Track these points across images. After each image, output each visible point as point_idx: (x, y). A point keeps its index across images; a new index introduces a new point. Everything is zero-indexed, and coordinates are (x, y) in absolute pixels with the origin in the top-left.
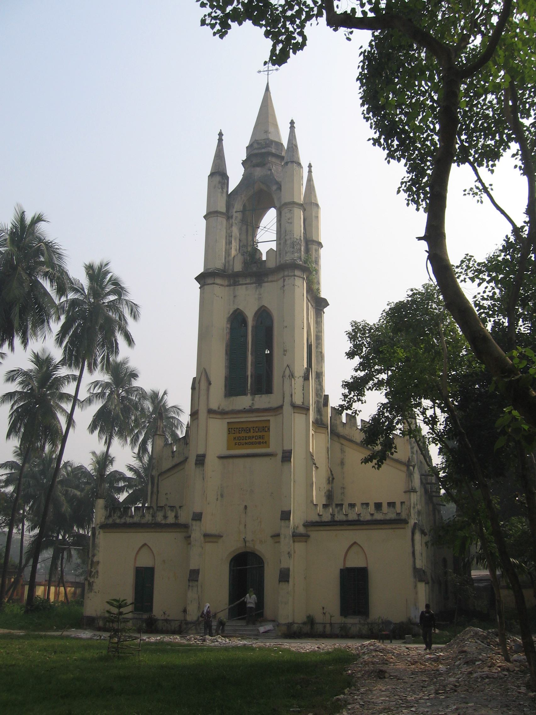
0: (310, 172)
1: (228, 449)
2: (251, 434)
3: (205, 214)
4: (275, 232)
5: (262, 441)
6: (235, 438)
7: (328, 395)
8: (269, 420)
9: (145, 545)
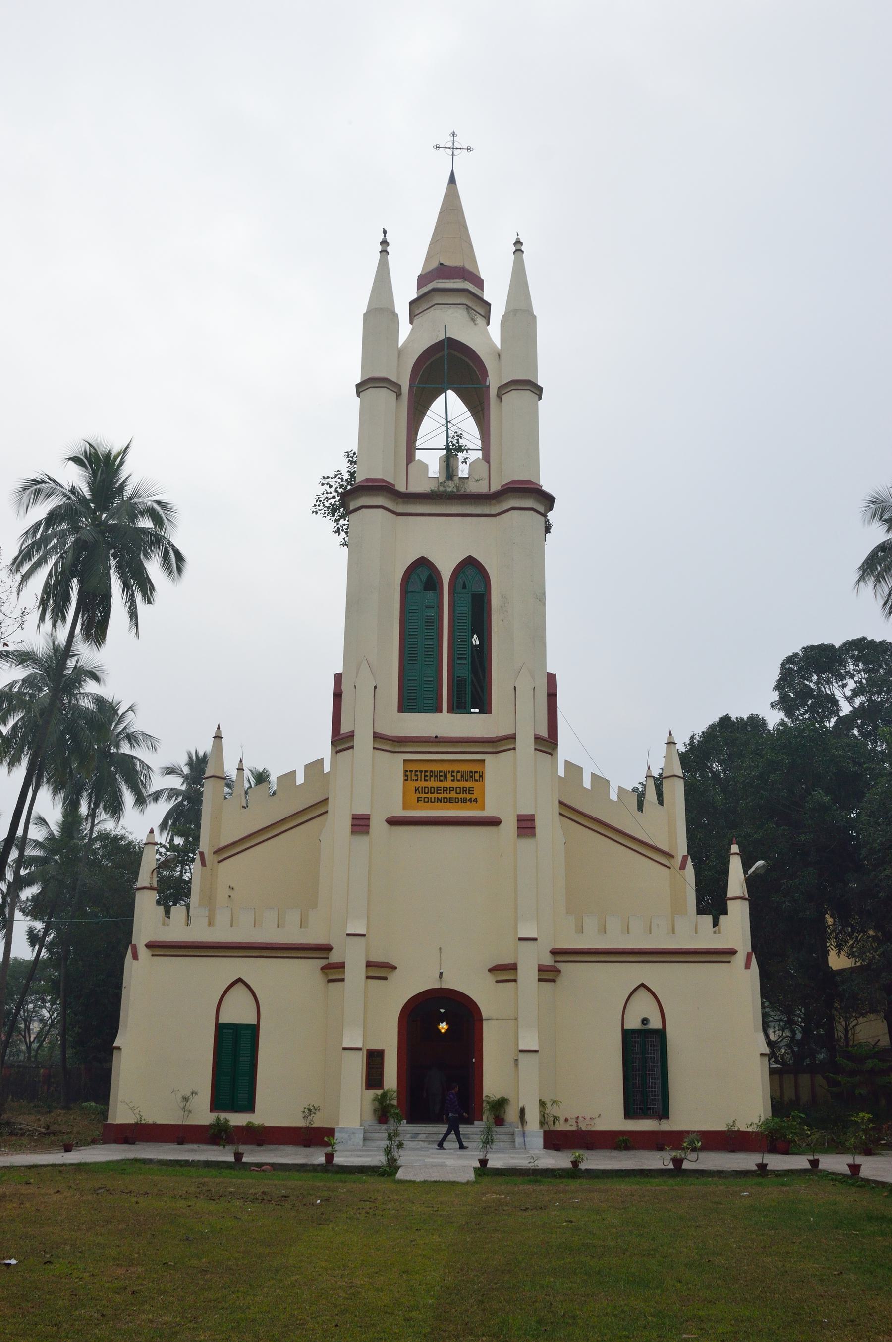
1: (405, 807)
2: (448, 784)
5: (468, 796)
6: (417, 789)
8: (483, 761)
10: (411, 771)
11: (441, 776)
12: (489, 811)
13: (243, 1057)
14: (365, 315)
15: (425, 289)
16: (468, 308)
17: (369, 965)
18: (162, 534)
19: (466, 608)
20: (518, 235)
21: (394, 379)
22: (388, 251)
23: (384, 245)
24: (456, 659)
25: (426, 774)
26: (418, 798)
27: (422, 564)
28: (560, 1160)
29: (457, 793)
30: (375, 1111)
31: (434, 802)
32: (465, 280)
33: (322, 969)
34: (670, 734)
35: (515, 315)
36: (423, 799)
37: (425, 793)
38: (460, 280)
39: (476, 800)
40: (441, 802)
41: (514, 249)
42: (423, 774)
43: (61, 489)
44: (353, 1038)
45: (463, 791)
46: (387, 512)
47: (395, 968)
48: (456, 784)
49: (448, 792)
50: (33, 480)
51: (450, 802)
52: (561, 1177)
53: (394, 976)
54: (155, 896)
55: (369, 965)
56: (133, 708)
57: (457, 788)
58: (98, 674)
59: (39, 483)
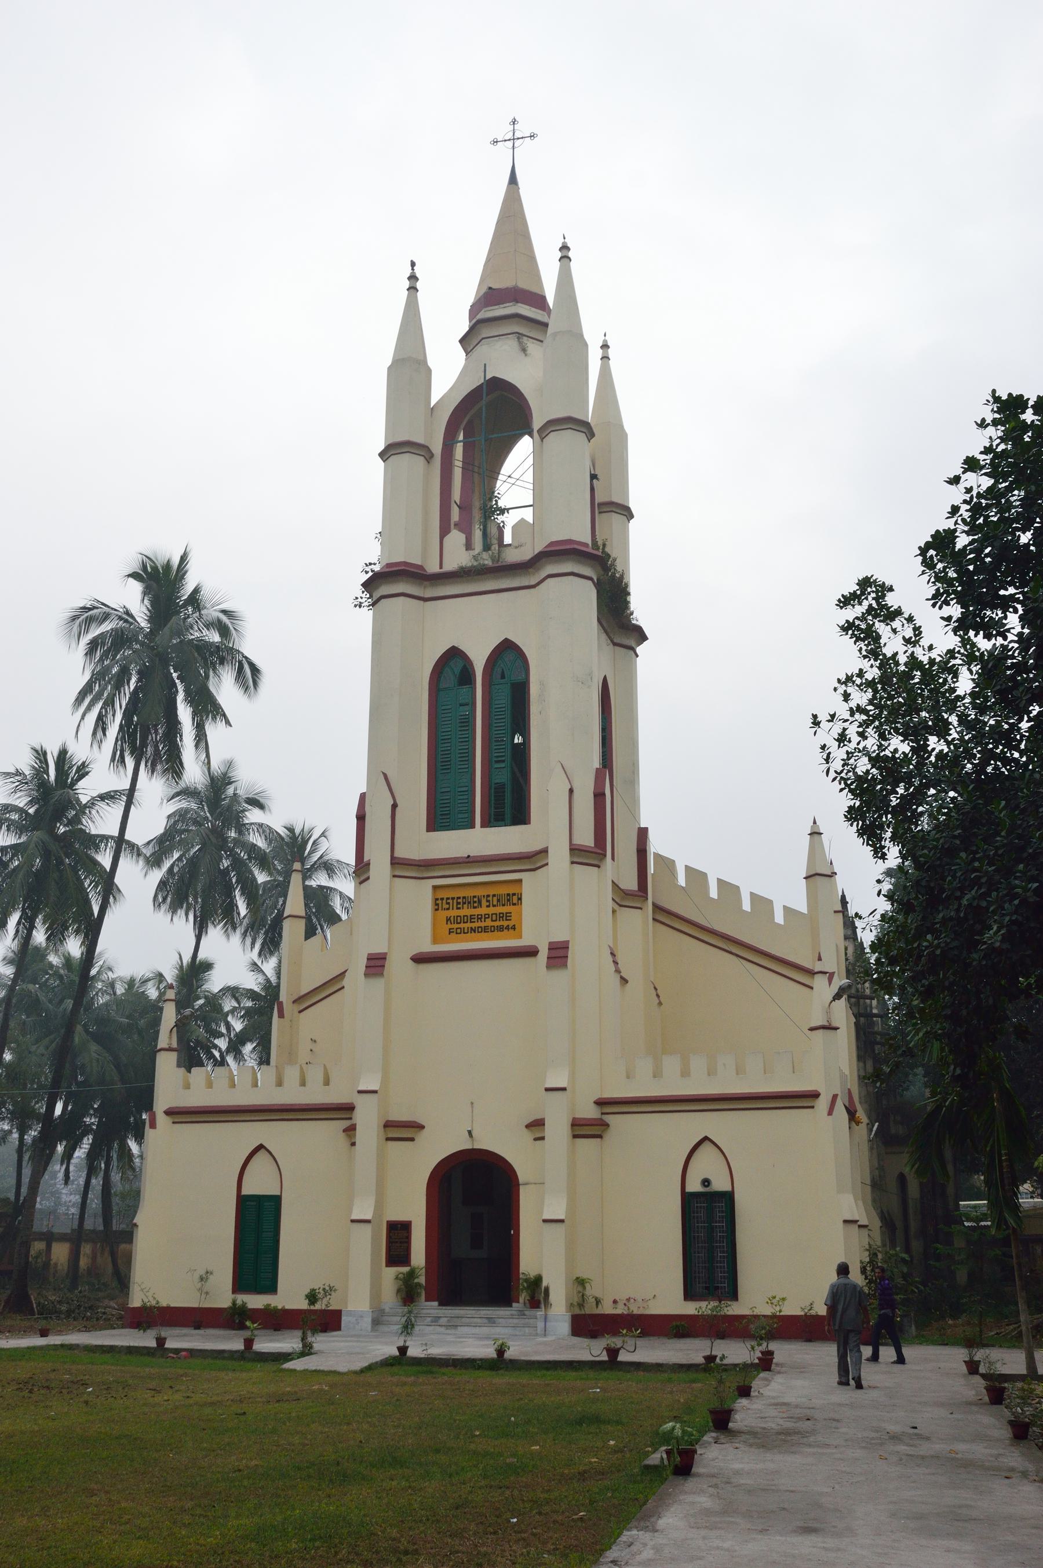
0: (605, 358)
1: (435, 940)
2: (483, 910)
3: (382, 447)
4: (531, 486)
5: (505, 923)
6: (448, 920)
7: (646, 829)
8: (520, 881)
9: (261, 1147)
10: (442, 899)
11: (475, 902)
12: (526, 940)
13: (267, 1232)
14: (389, 368)
15: (474, 321)
16: (520, 336)
17: (388, 1125)
18: (231, 645)
19: (504, 702)
20: (564, 238)
21: (420, 440)
22: (418, 287)
23: (412, 281)
24: (494, 762)
25: (459, 901)
26: (450, 929)
27: (454, 654)
28: (592, 1350)
29: (492, 921)
30: (398, 1291)
31: (468, 933)
32: (517, 302)
33: (344, 1131)
34: (815, 822)
35: (554, 339)
36: (455, 930)
37: (457, 923)
38: (511, 304)
39: (514, 928)
40: (475, 932)
41: (559, 255)
42: (455, 901)
43: (116, 612)
44: (364, 1209)
45: (500, 917)
46: (411, 599)
47: (422, 1127)
48: (492, 910)
49: (483, 920)
50: (81, 608)
51: (485, 932)
52: (480, 1368)
53: (422, 1137)
54: (174, 1056)
55: (388, 1125)
56: (326, 834)
57: (492, 914)
58: (261, 800)
59: (90, 609)
